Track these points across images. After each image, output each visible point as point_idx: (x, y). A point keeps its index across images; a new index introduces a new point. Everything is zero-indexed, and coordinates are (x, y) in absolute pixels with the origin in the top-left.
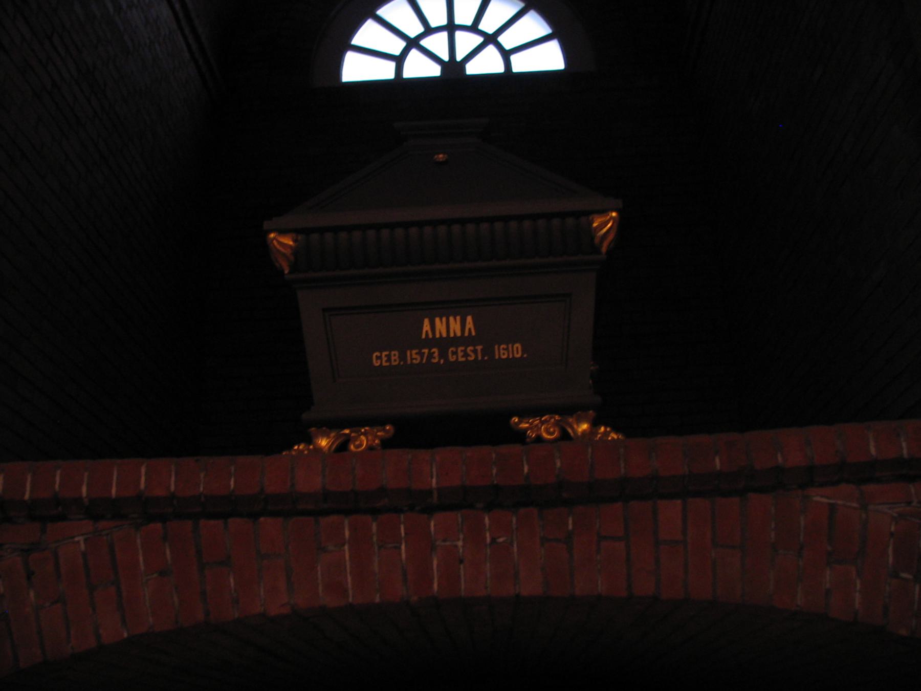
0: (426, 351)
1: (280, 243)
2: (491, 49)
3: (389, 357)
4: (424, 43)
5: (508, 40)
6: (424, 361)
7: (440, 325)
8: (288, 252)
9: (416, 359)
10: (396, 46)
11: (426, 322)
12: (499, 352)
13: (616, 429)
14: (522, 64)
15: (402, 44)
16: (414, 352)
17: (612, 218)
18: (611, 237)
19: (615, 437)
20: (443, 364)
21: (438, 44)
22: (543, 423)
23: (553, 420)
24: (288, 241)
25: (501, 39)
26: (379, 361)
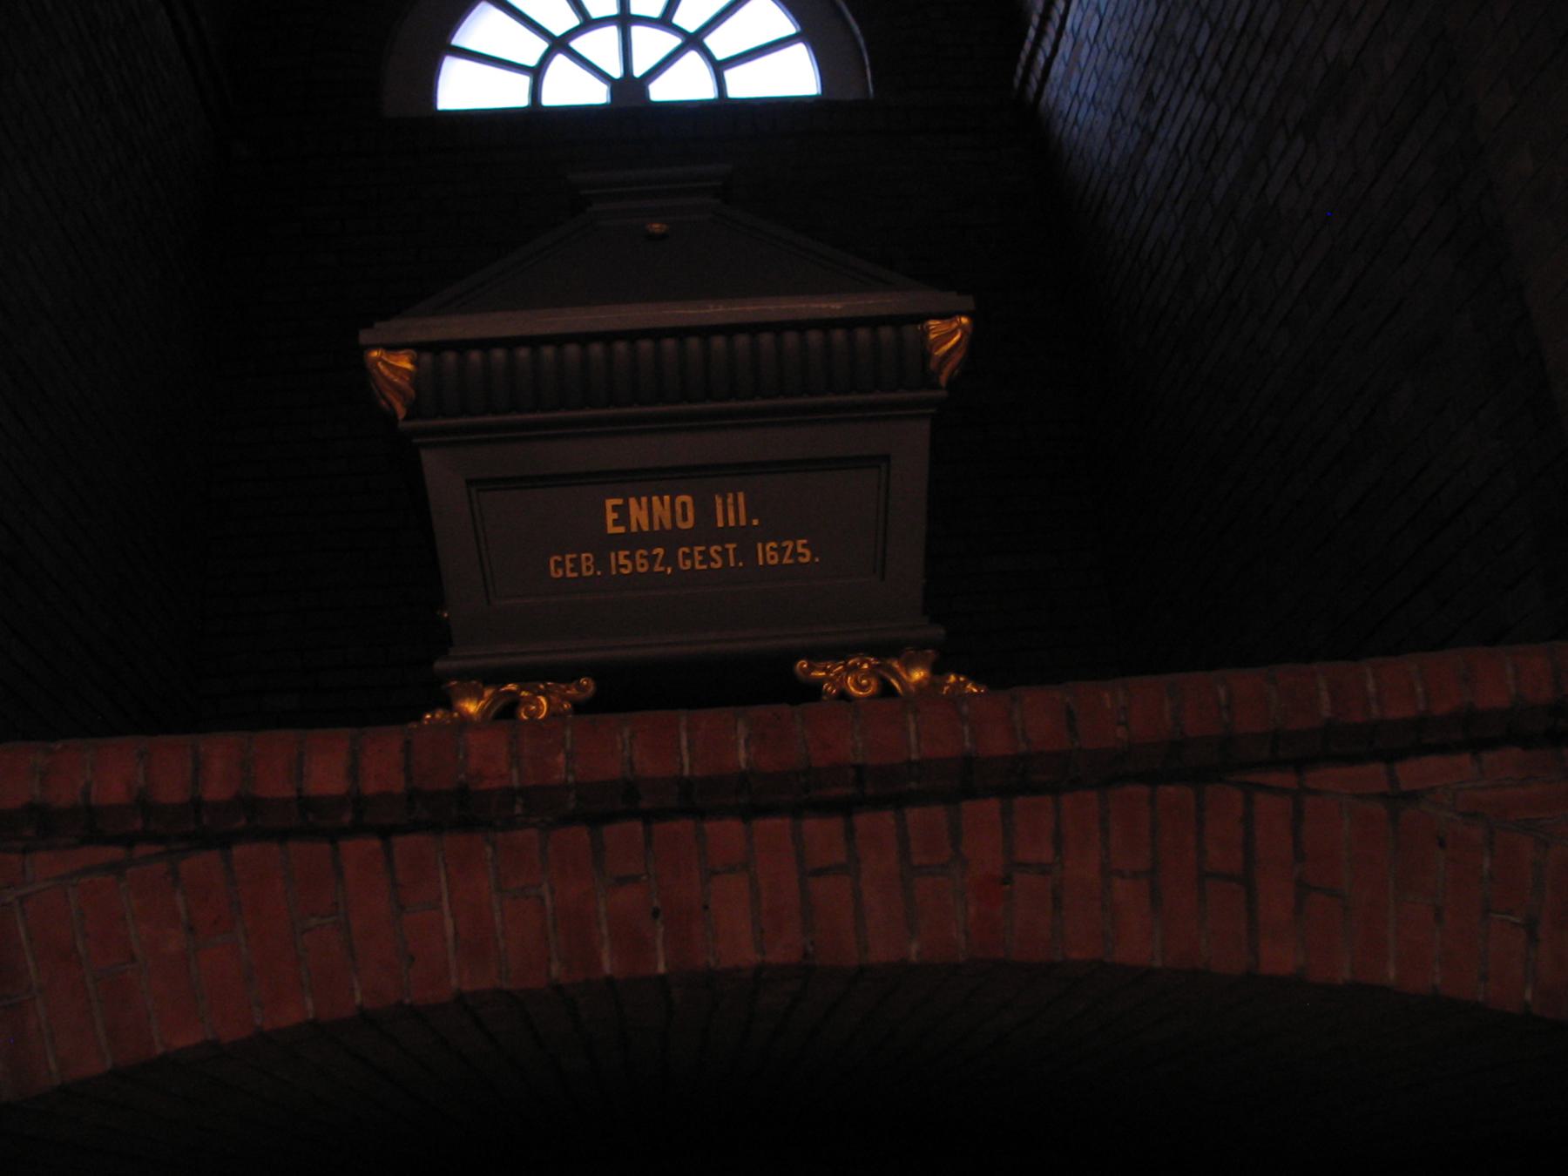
1: (385, 363)
2: (692, 58)
3: (577, 563)
4: (576, 44)
5: (722, 43)
7: (638, 515)
8: (404, 384)
9: (625, 566)
10: (530, 49)
13: (975, 677)
14: (745, 84)
15: (542, 45)
16: (622, 554)
17: (960, 326)
18: (958, 357)
20: (670, 575)
21: (601, 46)
22: (849, 670)
25: (710, 41)
26: (688, 563)
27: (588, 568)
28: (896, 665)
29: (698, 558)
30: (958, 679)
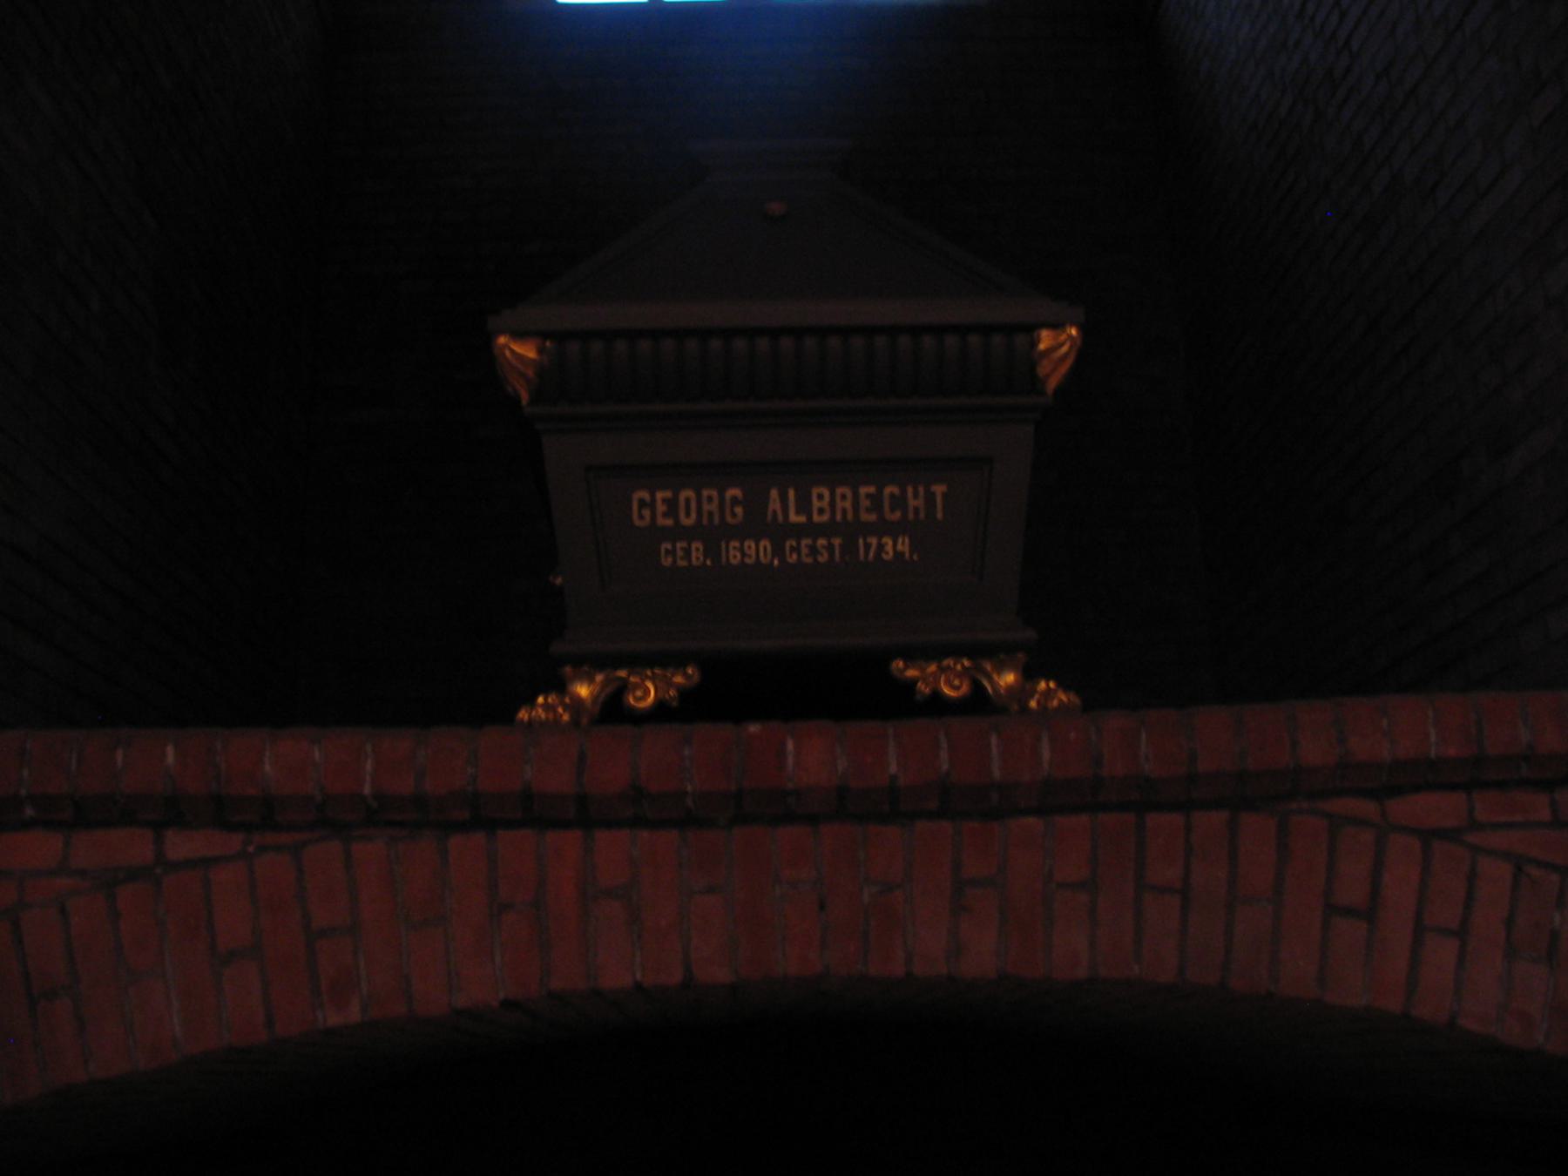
0: (874, 541)
1: (512, 351)
3: (687, 552)
6: (871, 554)
8: (530, 373)
11: (774, 493)
12: (727, 552)
13: (1064, 685)
18: (1070, 361)
19: (1064, 698)
22: (942, 670)
23: (959, 667)
24: (528, 351)
27: (698, 558)
28: (988, 667)
29: (805, 551)
30: (1048, 685)
